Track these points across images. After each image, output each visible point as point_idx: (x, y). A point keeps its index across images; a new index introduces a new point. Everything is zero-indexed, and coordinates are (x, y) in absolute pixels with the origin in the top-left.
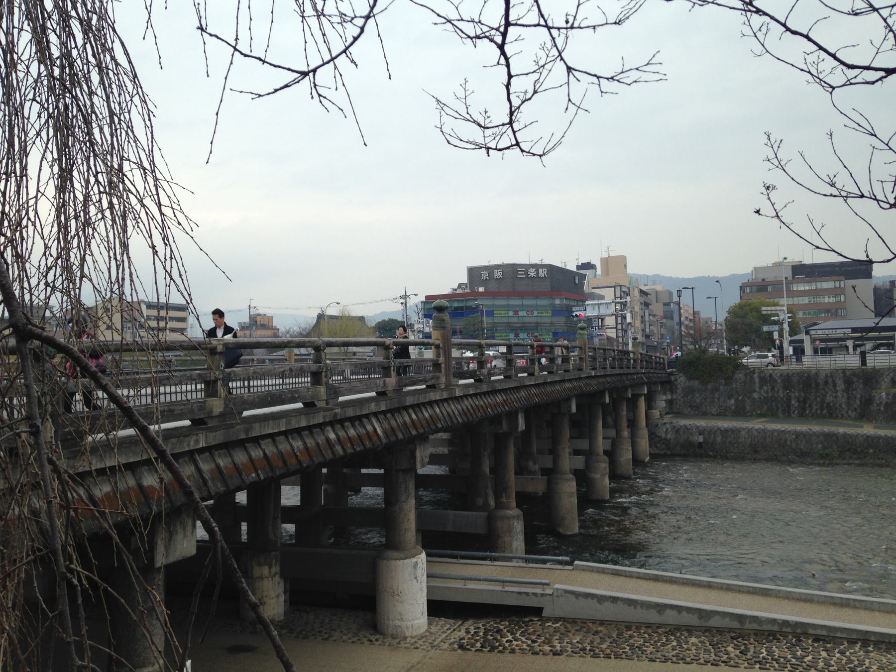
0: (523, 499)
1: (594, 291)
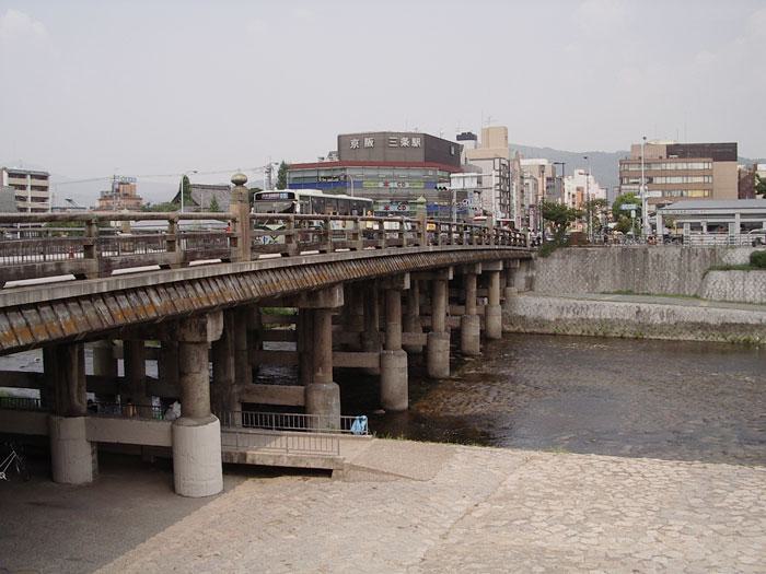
0: (340, 375)
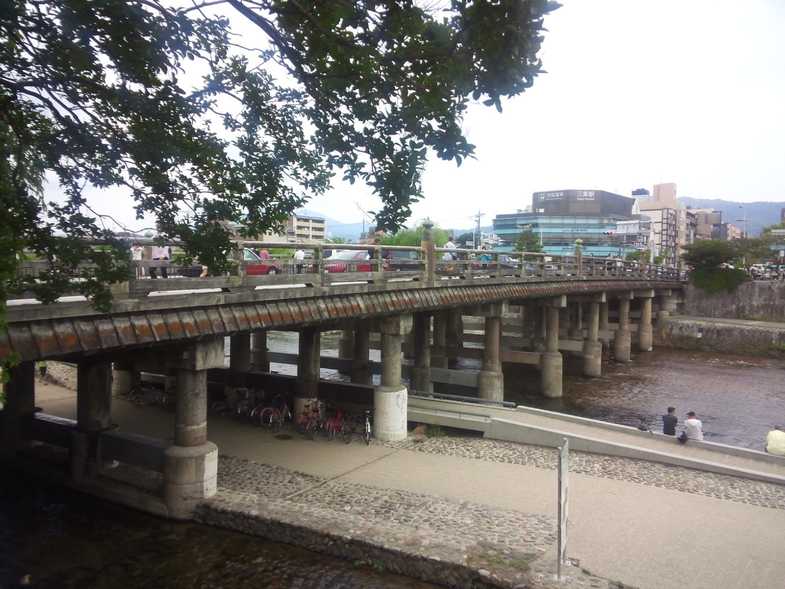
1: (643, 213)
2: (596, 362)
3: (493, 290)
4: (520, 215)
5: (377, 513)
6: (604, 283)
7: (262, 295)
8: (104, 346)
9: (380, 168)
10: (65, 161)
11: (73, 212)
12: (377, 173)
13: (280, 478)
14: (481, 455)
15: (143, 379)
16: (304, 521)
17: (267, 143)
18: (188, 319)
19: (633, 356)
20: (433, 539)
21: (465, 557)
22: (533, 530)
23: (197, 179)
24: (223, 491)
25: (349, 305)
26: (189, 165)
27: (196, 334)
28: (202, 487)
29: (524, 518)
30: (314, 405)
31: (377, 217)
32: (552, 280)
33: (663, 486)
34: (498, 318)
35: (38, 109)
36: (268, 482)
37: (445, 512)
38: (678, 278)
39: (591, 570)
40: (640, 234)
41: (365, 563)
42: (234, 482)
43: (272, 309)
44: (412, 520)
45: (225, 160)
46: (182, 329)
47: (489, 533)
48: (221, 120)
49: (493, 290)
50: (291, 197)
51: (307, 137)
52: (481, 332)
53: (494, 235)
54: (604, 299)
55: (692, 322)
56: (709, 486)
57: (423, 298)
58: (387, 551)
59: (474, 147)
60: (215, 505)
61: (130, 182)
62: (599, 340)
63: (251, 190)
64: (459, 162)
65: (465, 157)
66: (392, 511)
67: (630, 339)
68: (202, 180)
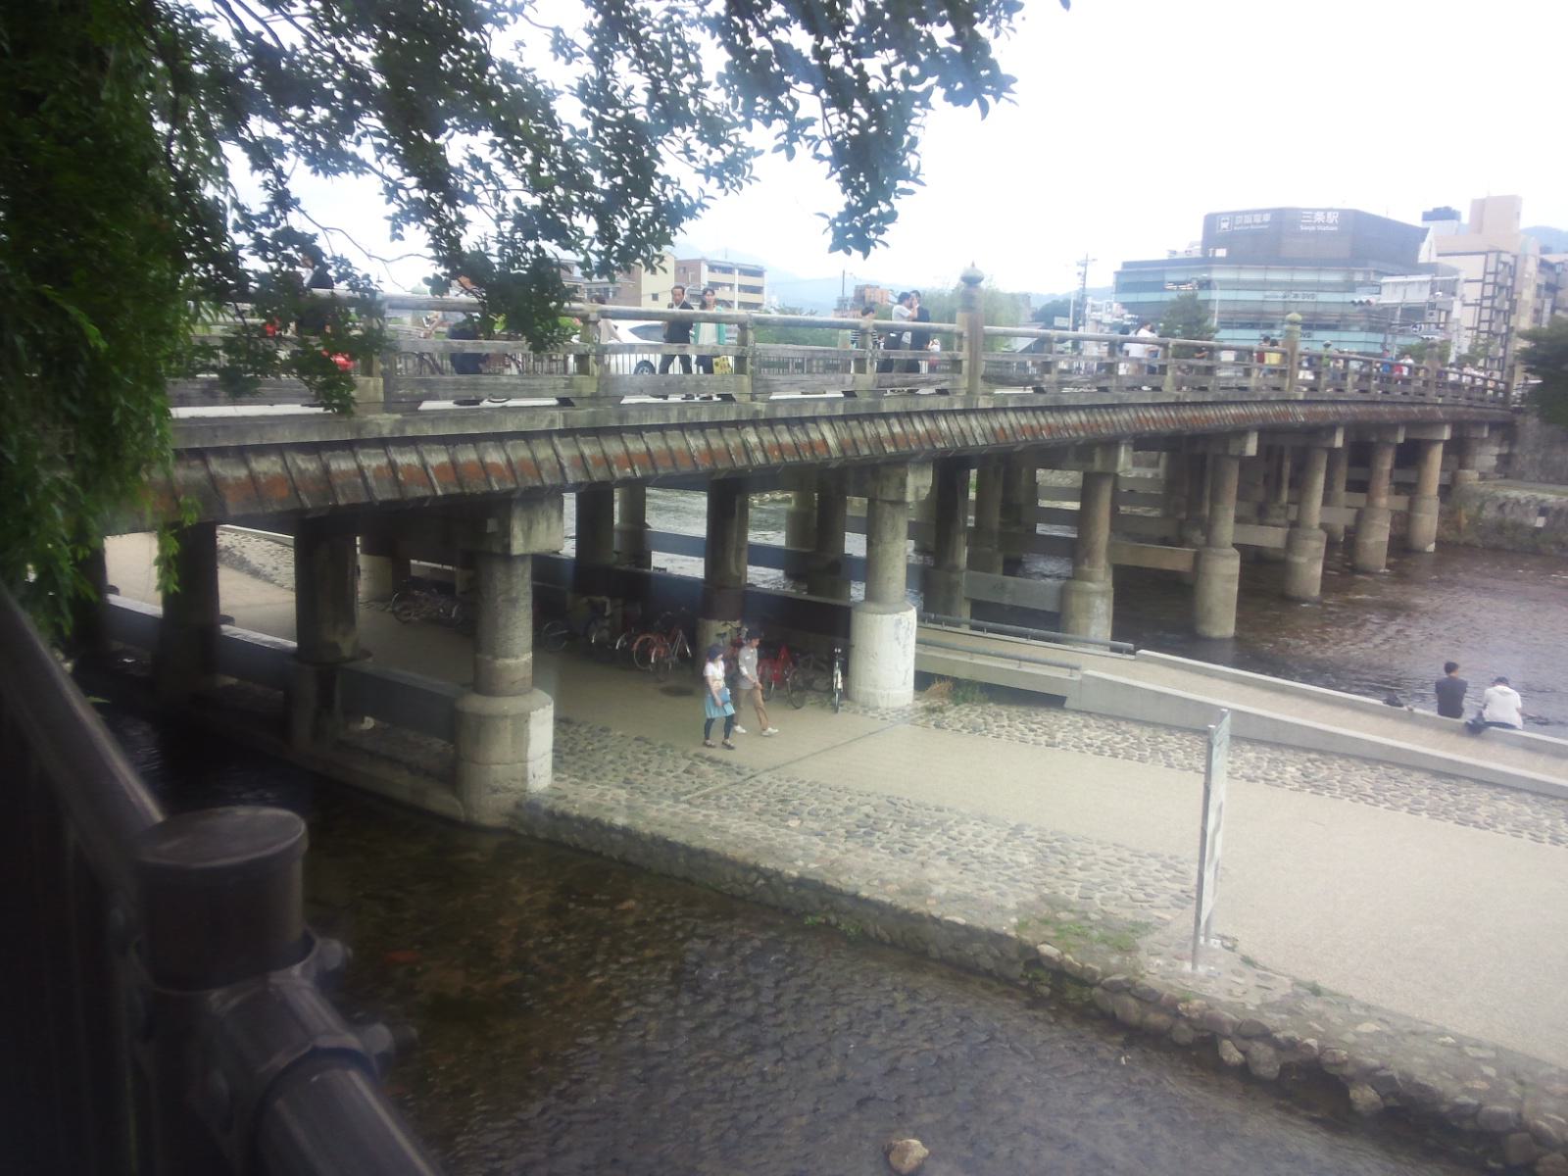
1: (1441, 260)
2: (1310, 569)
3: (1099, 418)
4: (1173, 263)
5: (849, 834)
6: (1341, 408)
7: (634, 413)
8: (342, 502)
9: (840, 125)
10: (259, 126)
11: (278, 224)
12: (833, 137)
13: (670, 764)
14: (1057, 740)
15: (414, 573)
16: (711, 841)
17: (632, 87)
18: (494, 457)
19: (1392, 560)
20: (954, 886)
21: (1014, 920)
22: (1150, 881)
23: (502, 165)
24: (563, 780)
25: (806, 439)
26: (486, 135)
27: (511, 486)
28: (525, 770)
29: (1135, 859)
30: (735, 634)
31: (832, 223)
32: (1230, 399)
33: (1424, 815)
34: (1108, 474)
35: (206, 21)
36: (646, 771)
37: (980, 841)
38: (1505, 402)
39: (1261, 959)
40: (1433, 306)
41: (824, 921)
42: (583, 767)
43: (655, 443)
44: (916, 850)
45: (553, 124)
46: (483, 475)
47: (1063, 882)
48: (545, 42)
49: (1102, 416)
50: (678, 198)
51: (709, 75)
52: (1075, 506)
53: (1115, 305)
54: (1339, 441)
55: (1528, 494)
56: (1519, 818)
57: (956, 430)
58: (866, 901)
59: (1014, 80)
60: (549, 804)
61: (377, 166)
62: (1323, 526)
63: (602, 183)
64: (984, 108)
65: (997, 101)
66: (878, 834)
67: (1388, 525)
68: (509, 164)
